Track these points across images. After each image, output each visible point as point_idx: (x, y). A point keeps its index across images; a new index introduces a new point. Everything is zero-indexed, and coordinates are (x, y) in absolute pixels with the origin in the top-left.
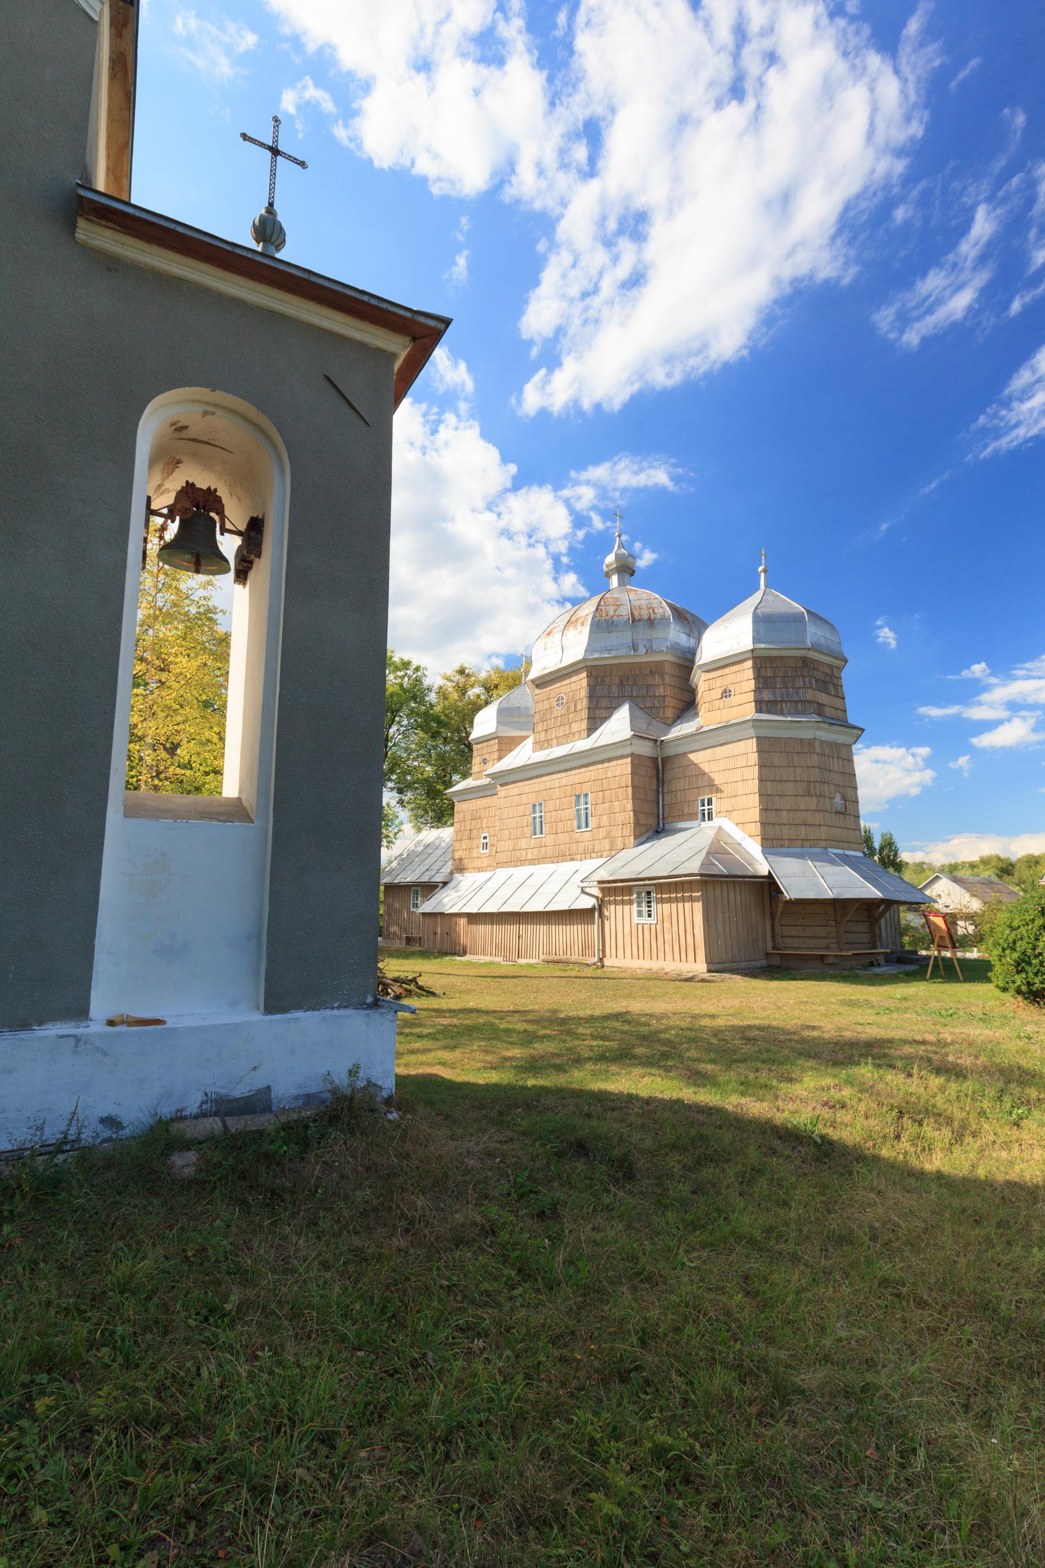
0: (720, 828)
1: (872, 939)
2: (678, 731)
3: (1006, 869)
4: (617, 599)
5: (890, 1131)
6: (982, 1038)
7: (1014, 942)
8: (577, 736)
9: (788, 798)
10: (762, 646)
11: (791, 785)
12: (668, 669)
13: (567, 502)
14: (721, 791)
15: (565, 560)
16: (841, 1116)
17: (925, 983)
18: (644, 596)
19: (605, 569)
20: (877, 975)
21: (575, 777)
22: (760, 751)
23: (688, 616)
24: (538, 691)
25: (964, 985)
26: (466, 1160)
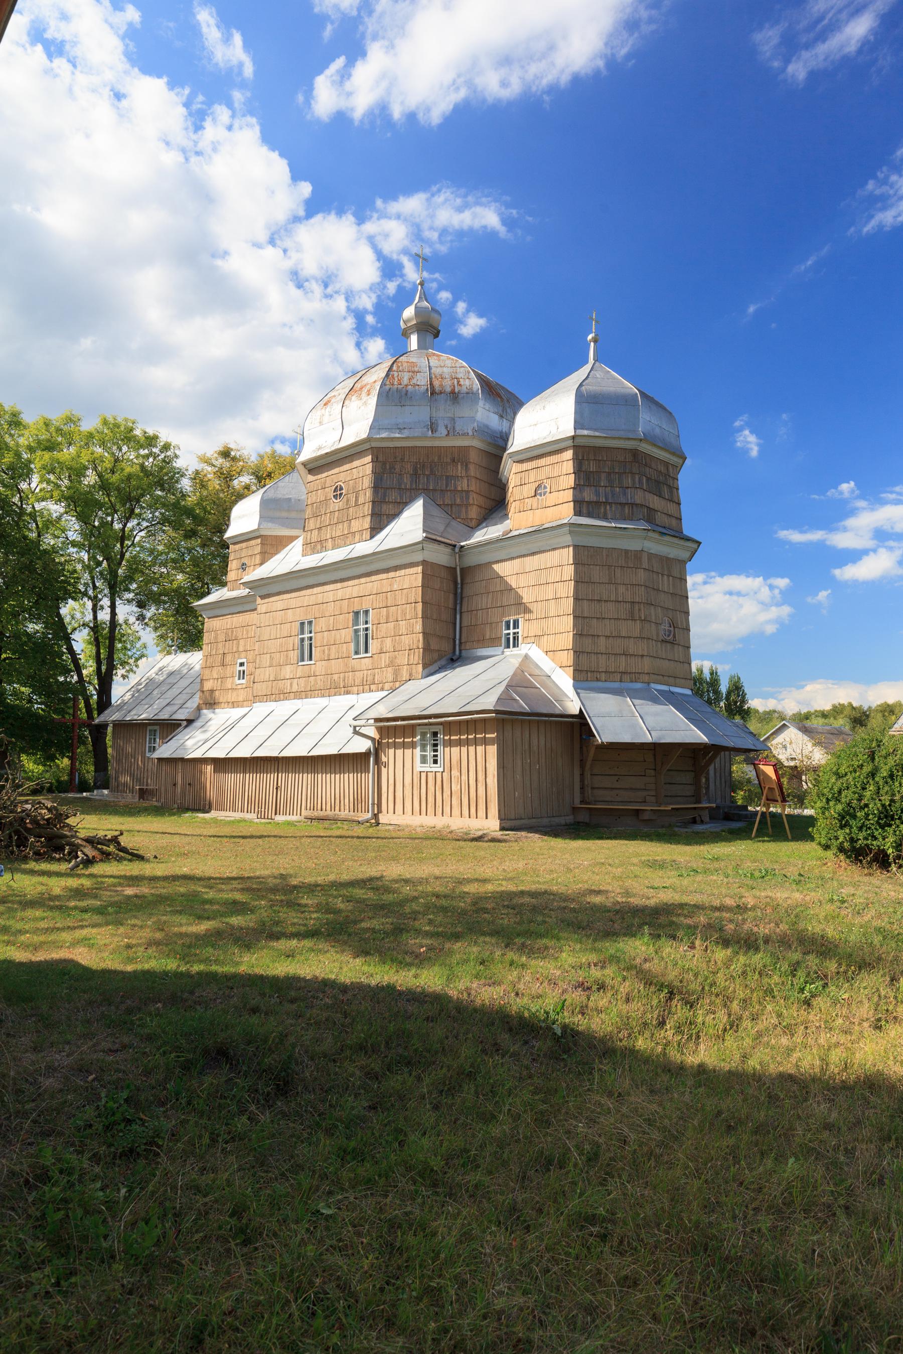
0: (526, 657)
1: (700, 789)
2: (481, 536)
3: (860, 718)
4: (414, 364)
5: (652, 1017)
6: (789, 902)
7: (840, 792)
8: (357, 537)
9: (607, 622)
10: (585, 432)
11: (611, 606)
12: (473, 457)
13: (371, 240)
14: (530, 611)
15: (370, 319)
16: (600, 1000)
17: (749, 842)
18: (449, 363)
19: (403, 326)
20: (697, 833)
21: (353, 588)
22: (577, 563)
23: (502, 393)
24: (310, 478)
25: (792, 843)
26: (41, 1079)
